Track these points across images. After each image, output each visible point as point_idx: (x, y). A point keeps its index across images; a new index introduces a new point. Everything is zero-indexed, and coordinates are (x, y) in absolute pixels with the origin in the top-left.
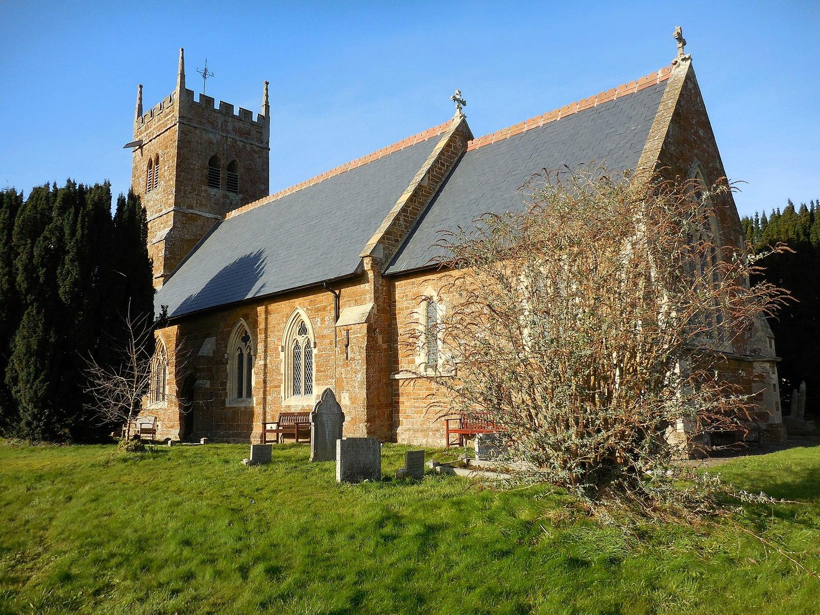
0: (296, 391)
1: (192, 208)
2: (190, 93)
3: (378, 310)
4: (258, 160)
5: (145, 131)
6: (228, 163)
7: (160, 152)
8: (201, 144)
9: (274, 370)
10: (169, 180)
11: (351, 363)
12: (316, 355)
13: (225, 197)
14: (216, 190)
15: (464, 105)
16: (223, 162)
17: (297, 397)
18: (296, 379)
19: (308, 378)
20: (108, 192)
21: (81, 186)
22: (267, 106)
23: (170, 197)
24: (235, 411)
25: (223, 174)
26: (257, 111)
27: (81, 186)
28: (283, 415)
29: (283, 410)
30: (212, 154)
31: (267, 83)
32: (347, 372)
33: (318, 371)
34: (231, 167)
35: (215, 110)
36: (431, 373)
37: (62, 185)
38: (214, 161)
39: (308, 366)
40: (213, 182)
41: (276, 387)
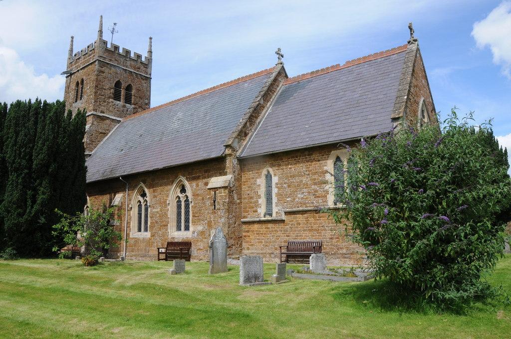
0: (179, 229)
1: (104, 113)
2: (105, 43)
3: (235, 179)
4: (144, 84)
5: (75, 64)
6: (126, 86)
7: (84, 78)
8: (111, 74)
9: (163, 215)
10: (90, 95)
11: (218, 212)
12: (192, 206)
13: (124, 106)
14: (119, 102)
15: (283, 57)
16: (124, 85)
17: (179, 233)
18: (179, 221)
19: (187, 221)
20: (64, 106)
21: (45, 101)
22: (150, 52)
23: (90, 105)
24: (136, 241)
25: (123, 92)
26: (144, 55)
27: (45, 103)
28: (170, 244)
29: (170, 241)
30: (117, 80)
31: (151, 38)
32: (215, 217)
33: (194, 216)
34: (129, 88)
35: (119, 54)
36: (268, 218)
37: (33, 101)
38: (118, 84)
39: (187, 213)
40: (117, 97)
41: (165, 226)
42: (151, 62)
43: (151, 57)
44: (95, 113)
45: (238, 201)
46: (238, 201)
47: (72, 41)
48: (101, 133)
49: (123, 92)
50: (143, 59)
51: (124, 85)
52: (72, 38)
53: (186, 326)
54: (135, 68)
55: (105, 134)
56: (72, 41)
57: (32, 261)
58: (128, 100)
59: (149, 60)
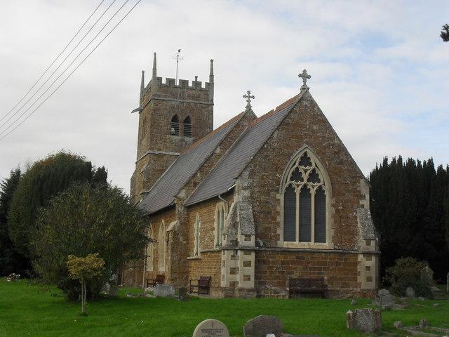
2: (160, 79)
13: (182, 140)
16: (181, 118)
22: (212, 76)
25: (181, 126)
26: (204, 80)
30: (174, 114)
34: (187, 120)
42: (213, 87)
43: (213, 80)
44: (151, 152)
45: (185, 242)
46: (185, 242)
47: (212, 65)
48: (158, 171)
49: (181, 126)
50: (203, 86)
51: (181, 118)
52: (212, 61)
53: (178, 335)
54: (193, 99)
55: (162, 171)
56: (212, 65)
57: (370, 223)
58: (187, 132)
59: (210, 85)
